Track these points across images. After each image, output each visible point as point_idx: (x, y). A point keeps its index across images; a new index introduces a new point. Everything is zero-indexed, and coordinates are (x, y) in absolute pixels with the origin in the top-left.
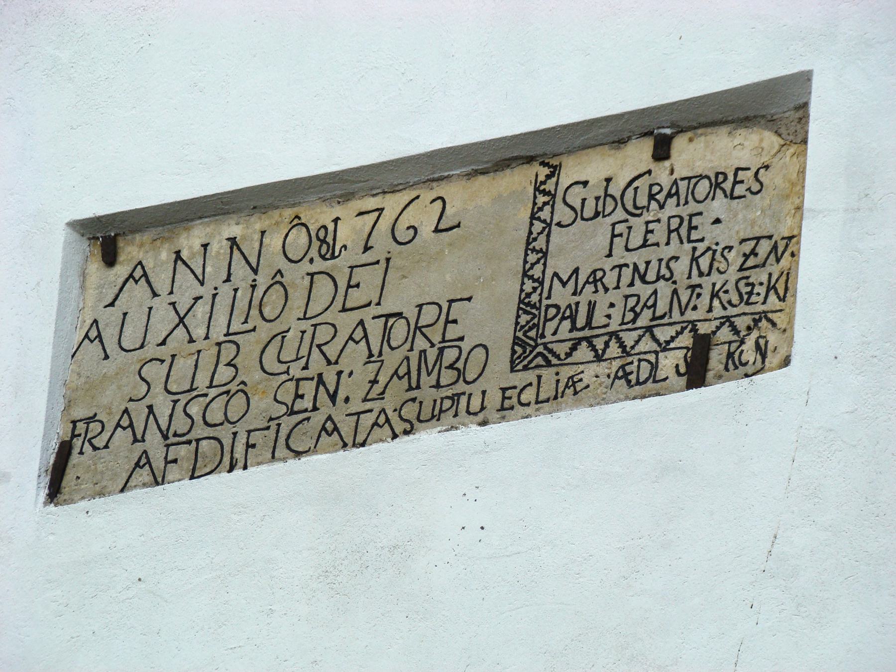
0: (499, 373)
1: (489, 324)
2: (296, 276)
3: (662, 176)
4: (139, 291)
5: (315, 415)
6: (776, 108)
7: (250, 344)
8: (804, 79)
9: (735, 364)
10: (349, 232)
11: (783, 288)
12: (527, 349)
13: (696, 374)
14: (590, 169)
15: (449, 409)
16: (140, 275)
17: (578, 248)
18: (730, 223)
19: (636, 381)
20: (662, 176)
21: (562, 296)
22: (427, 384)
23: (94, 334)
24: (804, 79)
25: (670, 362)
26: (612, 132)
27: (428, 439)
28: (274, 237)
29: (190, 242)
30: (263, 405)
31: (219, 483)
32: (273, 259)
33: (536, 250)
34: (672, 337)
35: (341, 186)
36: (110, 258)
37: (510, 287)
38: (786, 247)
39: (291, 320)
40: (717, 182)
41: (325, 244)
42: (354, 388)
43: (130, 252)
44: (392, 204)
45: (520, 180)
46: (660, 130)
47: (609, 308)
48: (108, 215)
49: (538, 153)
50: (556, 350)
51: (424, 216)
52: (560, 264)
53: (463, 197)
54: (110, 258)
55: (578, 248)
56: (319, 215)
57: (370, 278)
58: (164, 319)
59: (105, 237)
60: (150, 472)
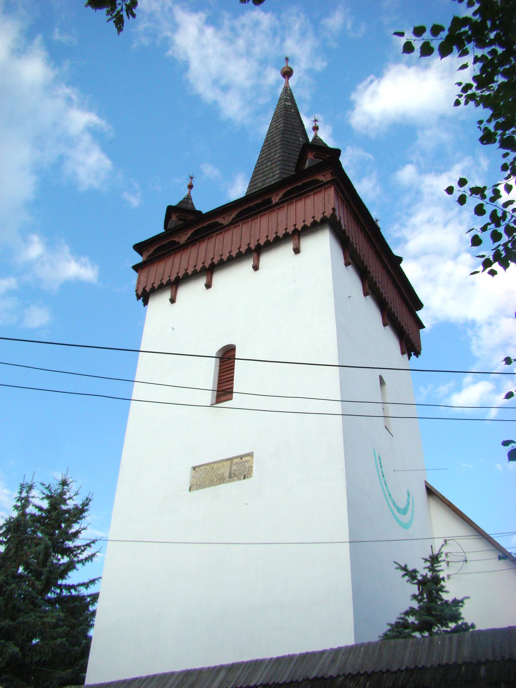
0: (228, 479)
1: (227, 475)
2: (210, 471)
3: (241, 461)
4: (197, 473)
5: (212, 483)
6: (251, 455)
7: (206, 477)
8: (253, 452)
9: (248, 477)
10: (215, 467)
11: (252, 471)
12: (230, 477)
13: (244, 478)
14: (235, 461)
15: (223, 482)
16: (197, 471)
17: (234, 468)
18: (247, 465)
19: (239, 479)
20: (241, 461)
21: (233, 472)
22: (221, 480)
23: (193, 477)
24: (253, 452)
25: (242, 477)
26: (237, 457)
27: (221, 485)
28: (208, 468)
29: (201, 468)
30: (207, 483)
31: (204, 490)
32: (208, 469)
33: (231, 468)
34: (90, 546)
35: (214, 463)
36: (194, 470)
37: (229, 471)
38: (252, 467)
39: (210, 476)
40: (246, 461)
41: (213, 468)
42: (215, 481)
43: (196, 469)
44: (218, 464)
45: (229, 462)
46: (241, 457)
47: (237, 473)
48: (290, 658)
49: (231, 459)
50: (232, 477)
51: (221, 465)
52: (233, 469)
53: (225, 463)
54: (194, 470)
55: (234, 468)
56: (212, 465)
57: (216, 471)
58: (199, 475)
59: (194, 468)
60: (198, 489)
